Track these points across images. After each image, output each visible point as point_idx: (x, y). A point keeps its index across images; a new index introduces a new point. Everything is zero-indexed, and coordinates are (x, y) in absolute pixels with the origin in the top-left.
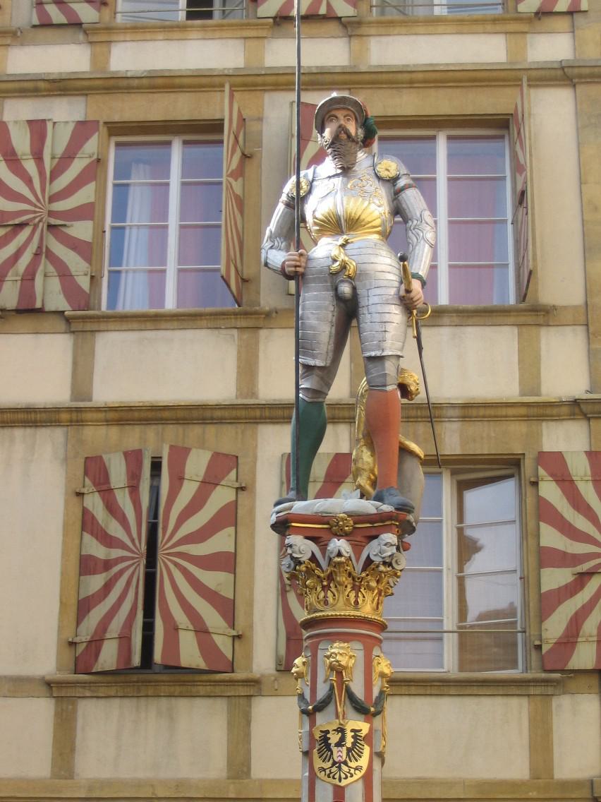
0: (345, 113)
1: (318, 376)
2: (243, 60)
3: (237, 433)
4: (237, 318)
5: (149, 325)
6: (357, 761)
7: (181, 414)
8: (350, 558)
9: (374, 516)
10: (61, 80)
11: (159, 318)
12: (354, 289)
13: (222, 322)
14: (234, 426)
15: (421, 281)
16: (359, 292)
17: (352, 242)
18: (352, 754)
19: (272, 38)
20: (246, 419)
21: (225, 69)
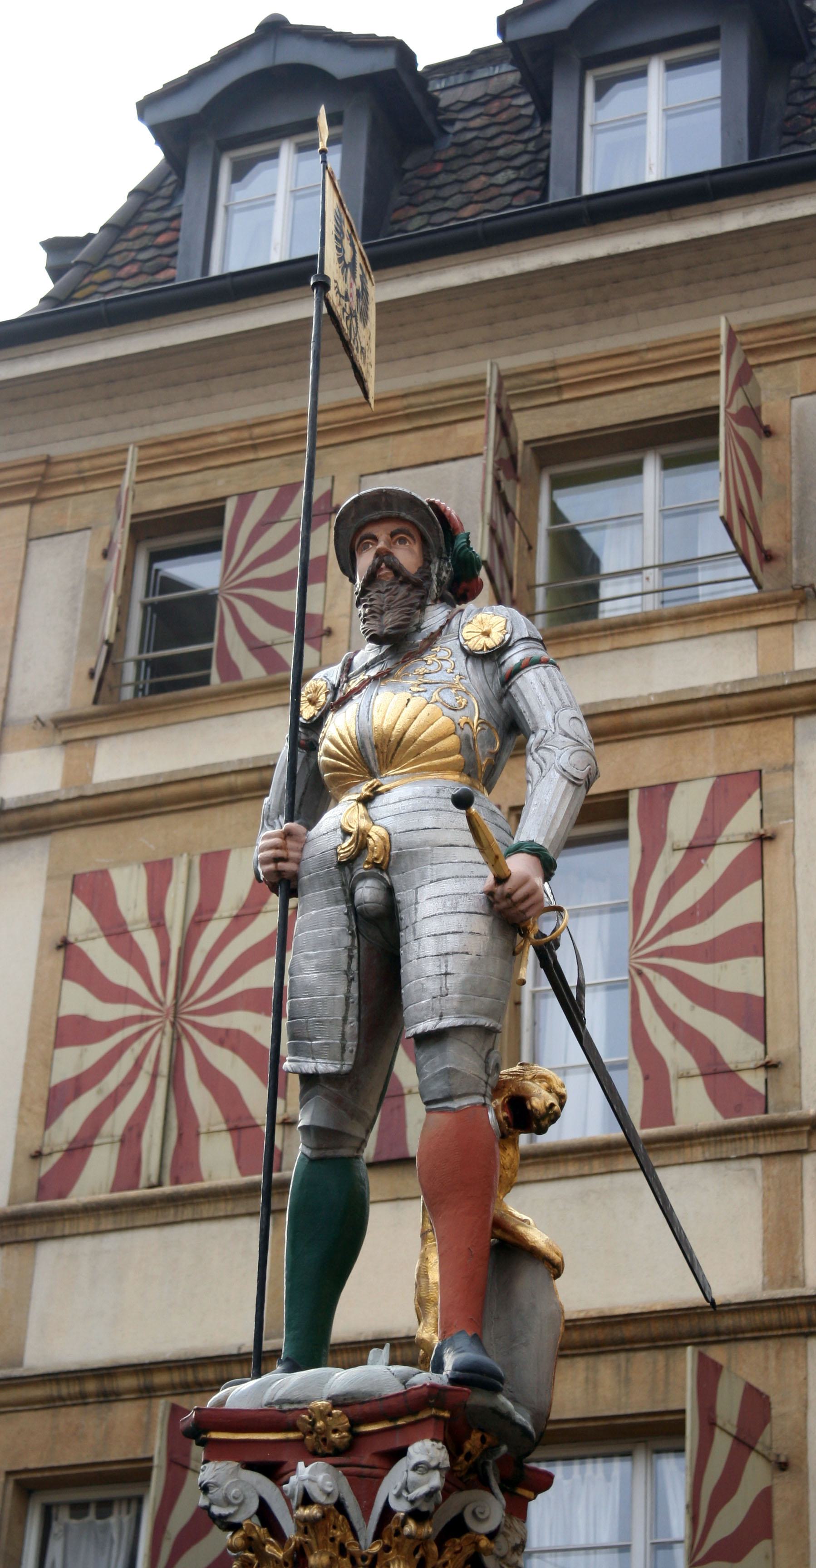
0: (393, 527)
1: (326, 1096)
2: (755, 667)
3: (767, 1358)
4: (758, 1137)
5: (597, 1165)
7: (657, 1328)
8: (340, 1506)
9: (392, 1402)
11: (614, 1151)
12: (390, 890)
13: (731, 1146)
14: (762, 1343)
15: (538, 856)
16: (399, 896)
17: (388, 790)
19: (807, 619)
20: (781, 1327)
21: (717, 685)
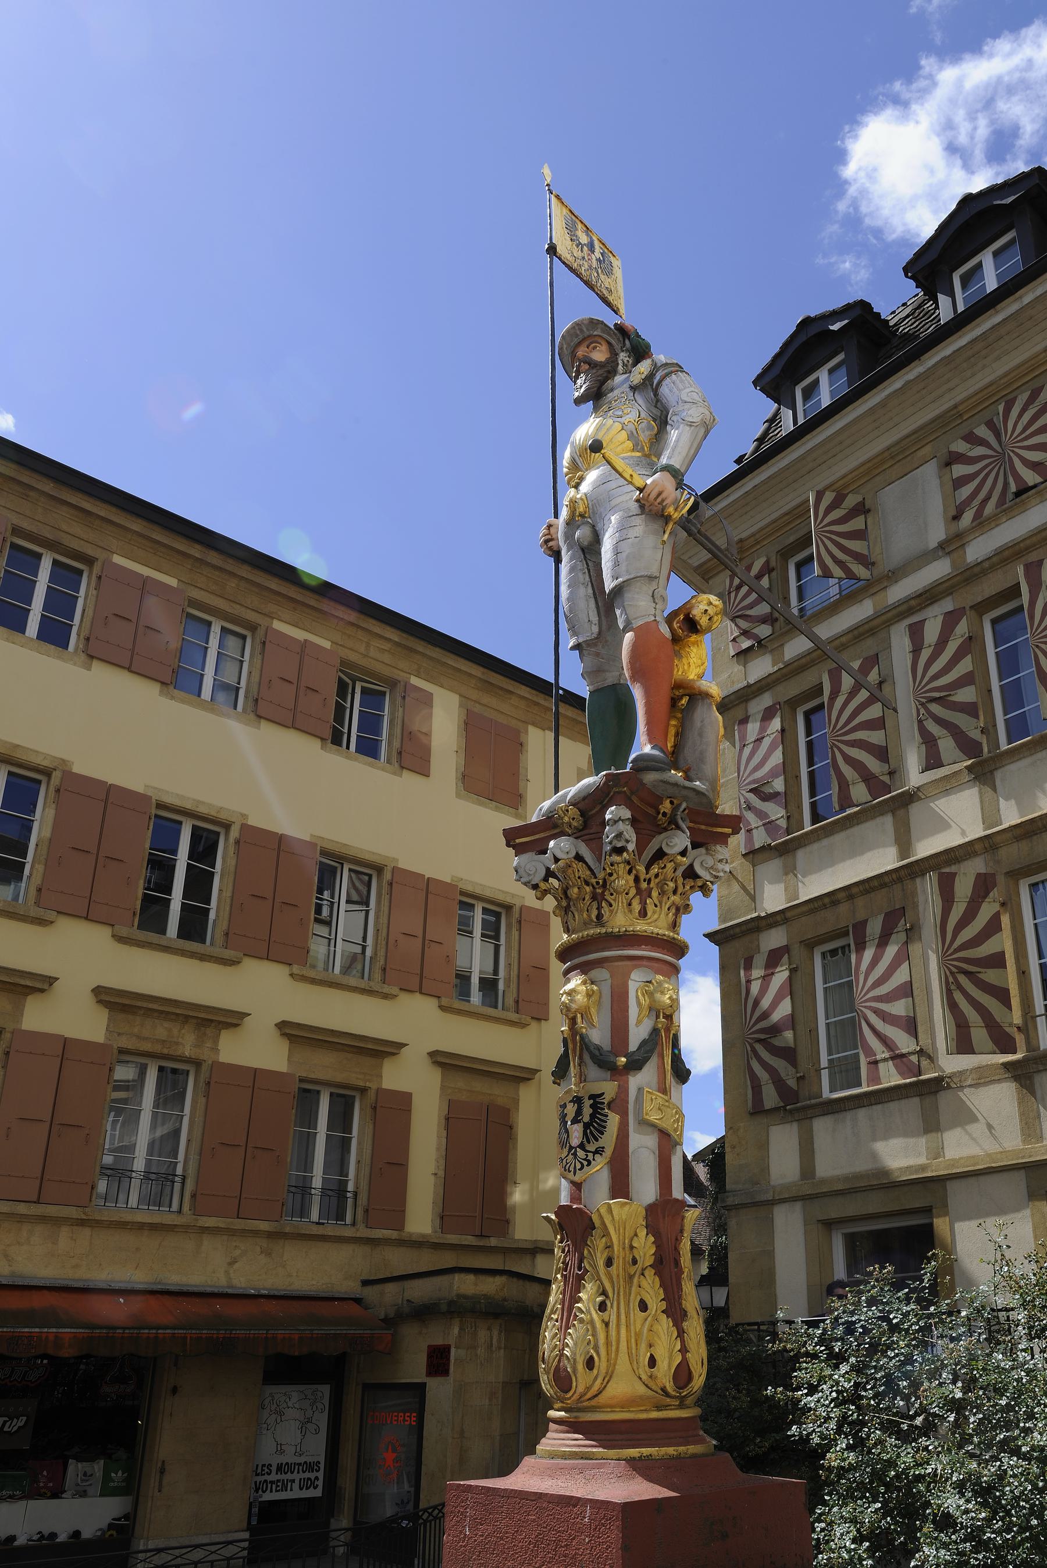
6: (597, 1140)
10: (926, 592)
15: (668, 471)
18: (591, 1132)
